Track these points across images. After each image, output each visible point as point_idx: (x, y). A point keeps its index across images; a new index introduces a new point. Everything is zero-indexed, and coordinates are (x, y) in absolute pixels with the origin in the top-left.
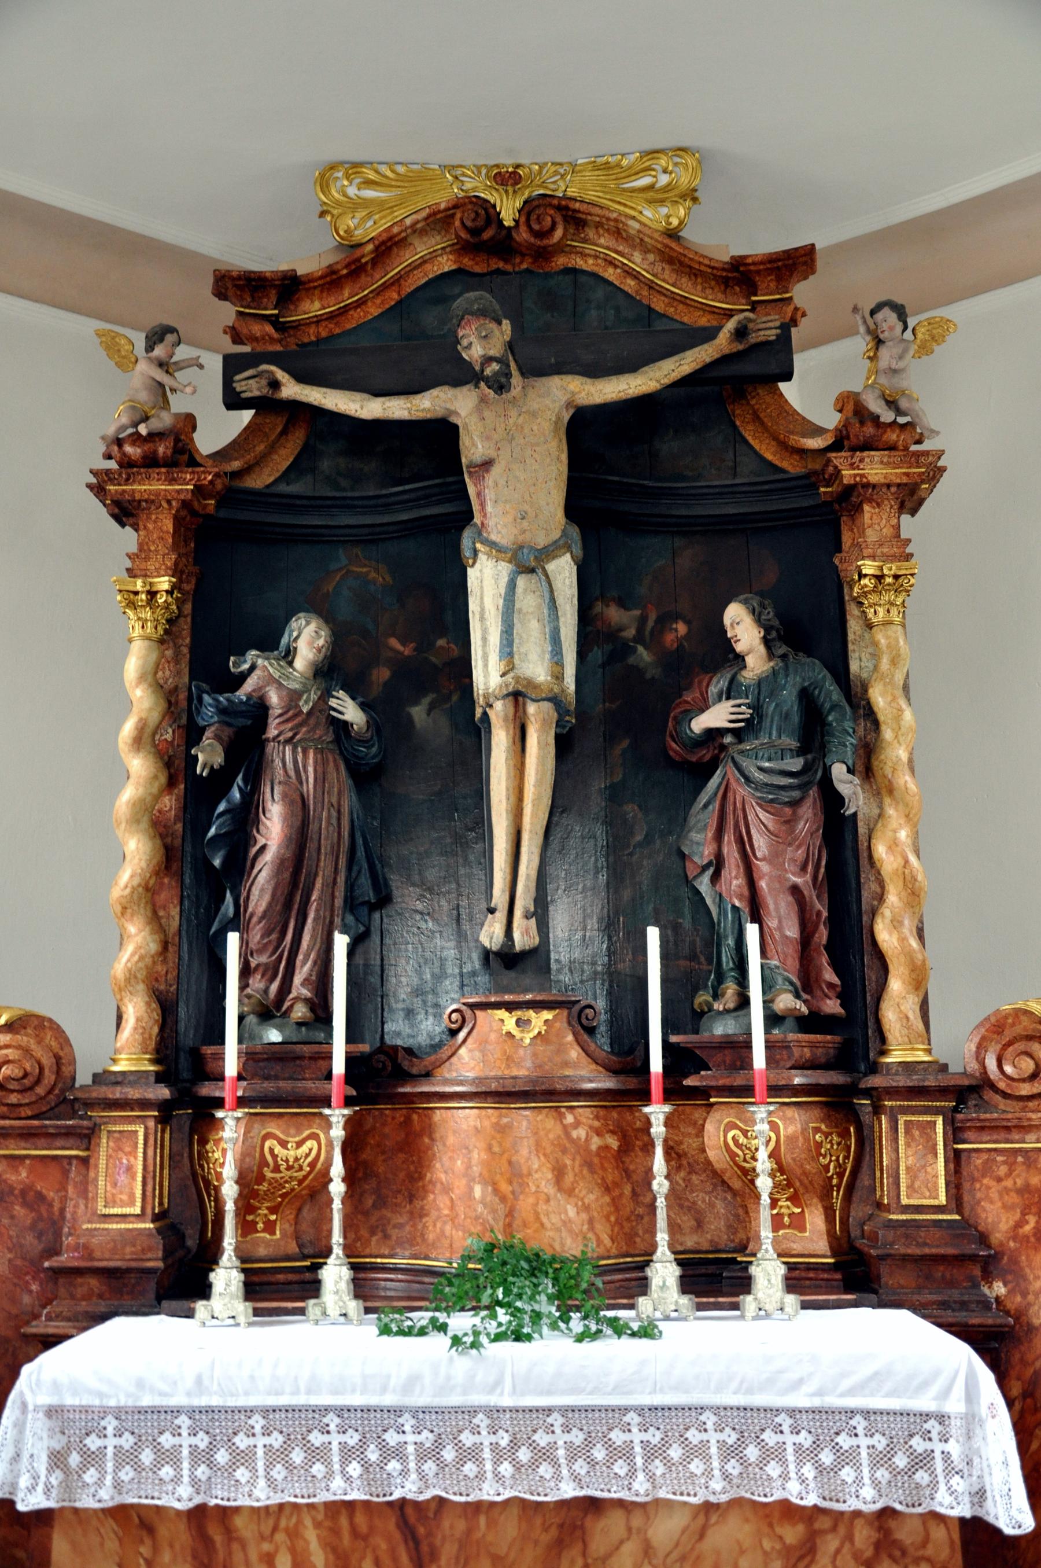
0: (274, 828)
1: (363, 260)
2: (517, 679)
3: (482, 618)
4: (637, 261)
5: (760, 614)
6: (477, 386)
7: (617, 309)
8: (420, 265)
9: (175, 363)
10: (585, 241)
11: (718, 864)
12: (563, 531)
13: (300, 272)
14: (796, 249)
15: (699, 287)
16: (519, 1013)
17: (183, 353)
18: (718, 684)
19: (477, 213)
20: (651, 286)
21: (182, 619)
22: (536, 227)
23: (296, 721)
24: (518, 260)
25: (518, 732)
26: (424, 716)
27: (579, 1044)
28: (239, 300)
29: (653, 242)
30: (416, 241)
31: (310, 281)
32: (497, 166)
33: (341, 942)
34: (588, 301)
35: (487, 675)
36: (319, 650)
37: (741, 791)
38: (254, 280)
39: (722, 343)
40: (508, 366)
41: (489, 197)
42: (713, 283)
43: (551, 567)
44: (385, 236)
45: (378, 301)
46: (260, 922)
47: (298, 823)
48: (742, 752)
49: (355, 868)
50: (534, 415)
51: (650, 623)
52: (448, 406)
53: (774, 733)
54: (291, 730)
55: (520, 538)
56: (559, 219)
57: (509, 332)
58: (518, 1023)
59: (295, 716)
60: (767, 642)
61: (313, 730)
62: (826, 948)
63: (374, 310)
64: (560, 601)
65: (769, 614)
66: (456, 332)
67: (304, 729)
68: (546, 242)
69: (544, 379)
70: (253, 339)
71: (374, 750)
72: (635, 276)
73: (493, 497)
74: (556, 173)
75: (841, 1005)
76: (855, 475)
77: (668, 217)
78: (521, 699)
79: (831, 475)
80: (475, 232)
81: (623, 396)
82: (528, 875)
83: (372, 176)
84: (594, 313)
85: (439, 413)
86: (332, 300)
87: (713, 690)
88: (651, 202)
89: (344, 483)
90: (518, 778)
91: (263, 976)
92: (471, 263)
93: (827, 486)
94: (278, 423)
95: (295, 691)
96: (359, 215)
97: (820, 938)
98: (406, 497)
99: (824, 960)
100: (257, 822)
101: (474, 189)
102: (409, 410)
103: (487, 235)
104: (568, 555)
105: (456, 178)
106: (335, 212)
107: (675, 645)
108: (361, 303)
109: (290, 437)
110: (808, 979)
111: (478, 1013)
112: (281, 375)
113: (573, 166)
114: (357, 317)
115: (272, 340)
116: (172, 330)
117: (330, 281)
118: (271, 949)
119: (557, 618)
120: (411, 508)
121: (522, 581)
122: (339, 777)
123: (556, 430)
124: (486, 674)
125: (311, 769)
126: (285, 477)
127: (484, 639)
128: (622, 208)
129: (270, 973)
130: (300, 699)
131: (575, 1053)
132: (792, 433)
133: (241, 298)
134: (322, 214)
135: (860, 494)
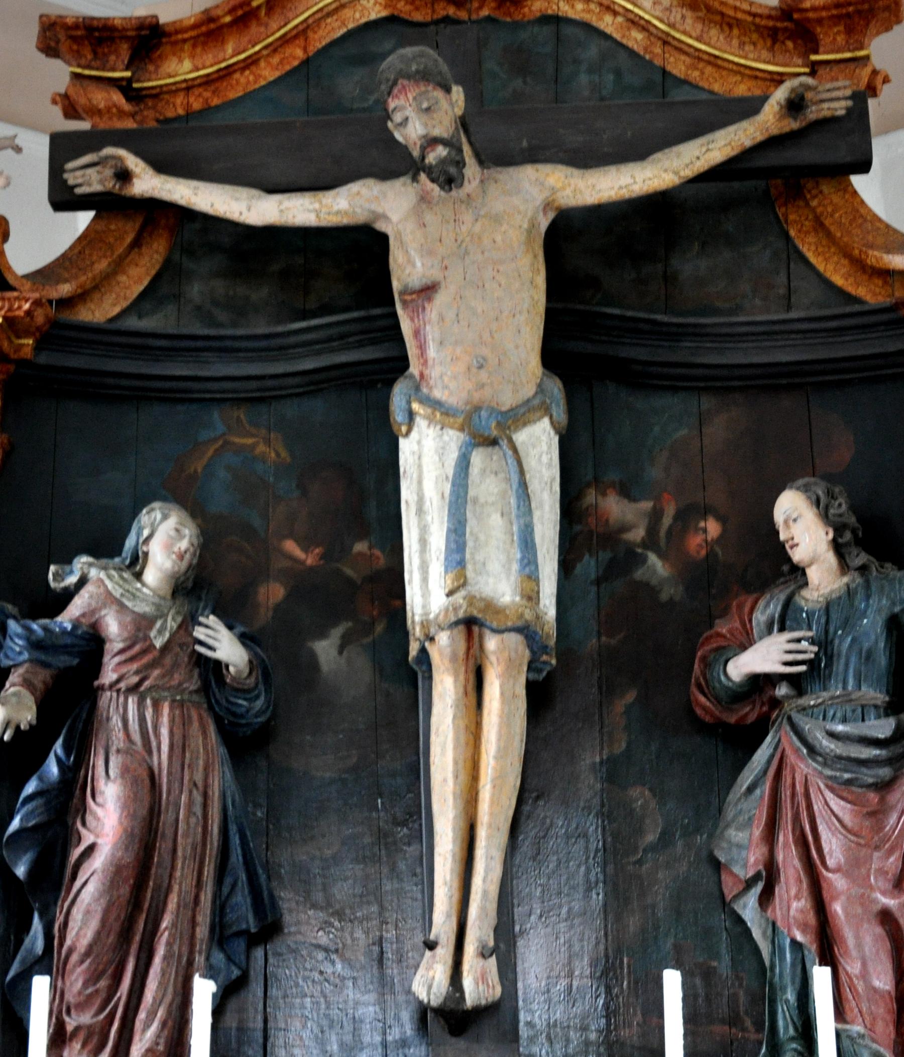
0: (107, 819)
2: (471, 600)
6: (415, 179)
7: (618, 73)
11: (768, 879)
15: (735, 42)
18: (767, 609)
20: (666, 41)
26: (334, 652)
28: (76, 57)
31: (177, 32)
33: (204, 991)
34: (576, 62)
35: (427, 594)
36: (181, 557)
37: (803, 768)
38: (97, 29)
39: (768, 120)
40: (460, 151)
42: (755, 36)
43: (521, 437)
45: (275, 60)
46: (82, 962)
47: (143, 812)
48: (803, 710)
49: (228, 881)
50: (497, 219)
51: (667, 521)
54: (137, 672)
55: (477, 396)
59: (144, 652)
60: (838, 547)
61: (169, 673)
63: (268, 73)
64: (534, 486)
65: (840, 506)
66: (385, 102)
67: (156, 673)
69: (511, 170)
70: (93, 112)
73: (437, 335)
78: (476, 629)
81: (626, 194)
85: (360, 217)
86: (209, 58)
87: (760, 617)
89: (222, 316)
90: (471, 746)
91: (84, 1046)
94: (129, 230)
100: (83, 809)
104: (546, 422)
107: (703, 553)
108: (251, 63)
109: (144, 249)
112: (133, 162)
114: (244, 83)
115: (122, 114)
118: (98, 1002)
119: (530, 511)
120: (319, 353)
121: (478, 458)
122: (207, 742)
123: (529, 241)
124: (426, 592)
125: (165, 732)
126: (136, 306)
127: (423, 542)
129: (95, 1040)
132: (871, 247)
133: (78, 54)
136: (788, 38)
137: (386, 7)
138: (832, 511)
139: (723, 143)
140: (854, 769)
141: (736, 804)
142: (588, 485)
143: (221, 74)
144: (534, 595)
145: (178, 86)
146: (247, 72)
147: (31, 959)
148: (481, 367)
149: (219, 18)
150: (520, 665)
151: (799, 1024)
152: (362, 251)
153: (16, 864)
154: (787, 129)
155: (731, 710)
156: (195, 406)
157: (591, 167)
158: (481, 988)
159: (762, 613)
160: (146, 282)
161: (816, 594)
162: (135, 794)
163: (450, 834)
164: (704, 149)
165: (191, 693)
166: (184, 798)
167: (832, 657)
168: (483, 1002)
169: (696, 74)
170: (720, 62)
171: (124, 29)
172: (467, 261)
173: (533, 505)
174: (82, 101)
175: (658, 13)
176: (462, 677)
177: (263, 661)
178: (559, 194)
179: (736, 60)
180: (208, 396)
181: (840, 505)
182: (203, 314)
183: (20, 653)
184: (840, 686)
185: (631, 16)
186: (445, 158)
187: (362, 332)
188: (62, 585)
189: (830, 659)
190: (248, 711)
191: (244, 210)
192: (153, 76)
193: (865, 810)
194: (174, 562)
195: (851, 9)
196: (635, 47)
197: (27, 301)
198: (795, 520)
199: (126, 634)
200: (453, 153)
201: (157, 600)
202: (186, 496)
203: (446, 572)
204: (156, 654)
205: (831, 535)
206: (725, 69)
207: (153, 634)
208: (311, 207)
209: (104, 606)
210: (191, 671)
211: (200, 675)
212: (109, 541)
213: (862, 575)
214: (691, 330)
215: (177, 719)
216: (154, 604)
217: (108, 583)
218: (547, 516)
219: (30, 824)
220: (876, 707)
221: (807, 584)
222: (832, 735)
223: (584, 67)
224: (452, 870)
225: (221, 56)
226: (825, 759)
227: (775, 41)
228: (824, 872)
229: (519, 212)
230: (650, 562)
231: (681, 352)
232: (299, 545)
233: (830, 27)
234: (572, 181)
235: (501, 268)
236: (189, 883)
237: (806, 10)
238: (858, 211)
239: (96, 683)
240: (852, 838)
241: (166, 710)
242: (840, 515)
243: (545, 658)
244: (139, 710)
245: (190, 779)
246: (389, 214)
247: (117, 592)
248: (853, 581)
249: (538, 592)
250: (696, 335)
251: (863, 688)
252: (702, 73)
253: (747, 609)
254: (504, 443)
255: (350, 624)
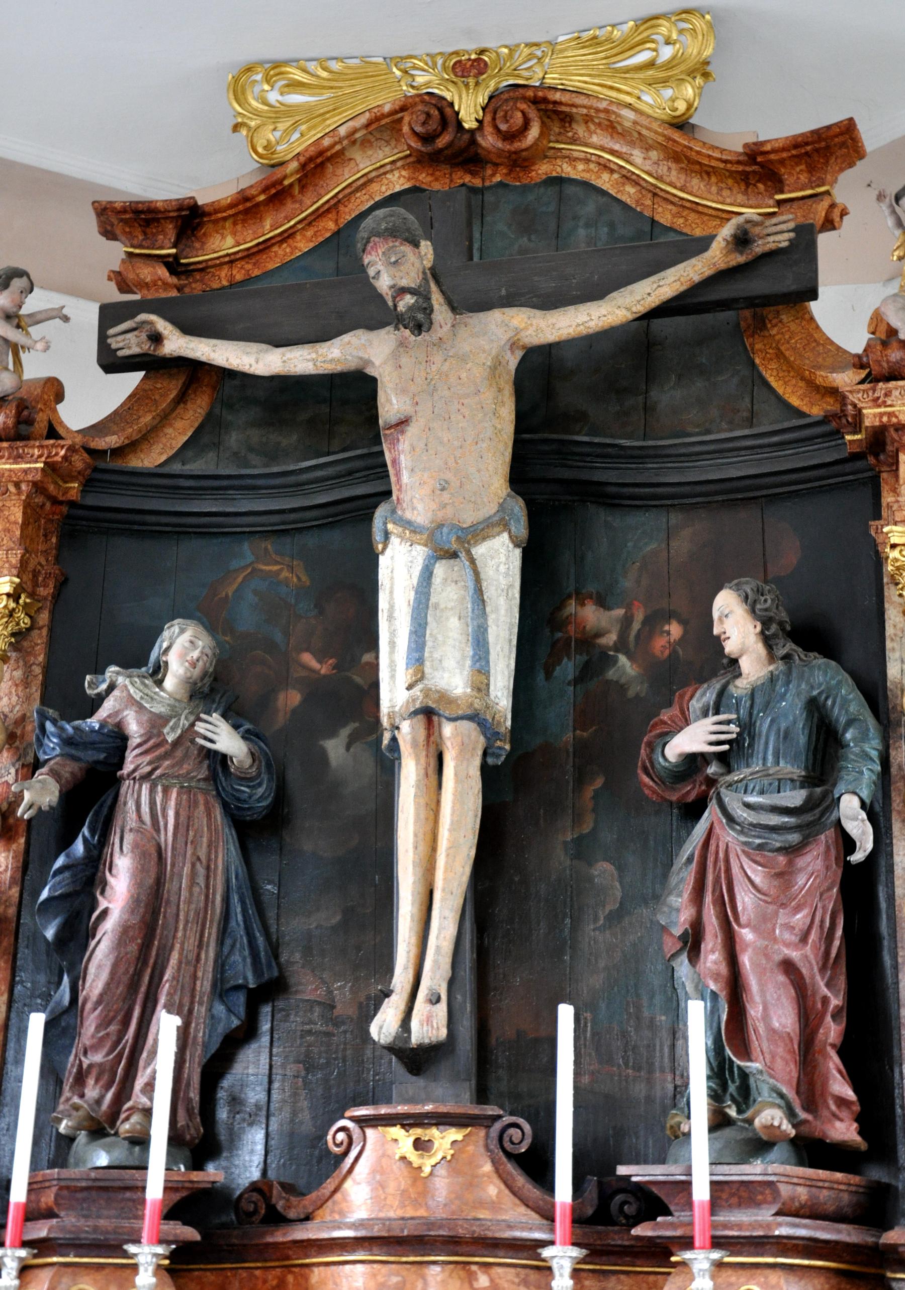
1: (286, 182)
2: (427, 692)
3: (391, 618)
4: (640, 162)
5: (755, 602)
7: (612, 226)
8: (364, 185)
9: (30, 316)
10: (574, 141)
11: (692, 942)
12: (501, 505)
13: (200, 202)
14: (828, 128)
15: (714, 189)
16: (417, 1132)
17: (34, 303)
18: (706, 695)
19: (428, 115)
20: (655, 194)
21: (35, 632)
22: (503, 127)
23: (157, 753)
24: (489, 172)
25: (433, 762)
26: (342, 750)
27: (500, 1176)
29: (652, 135)
30: (356, 154)
31: (216, 211)
32: (456, 53)
34: (576, 218)
35: (394, 693)
36: (194, 665)
37: (728, 837)
38: (142, 212)
39: (716, 256)
40: (428, 299)
41: (448, 96)
42: (730, 182)
43: (480, 551)
44: (312, 151)
45: (309, 233)
46: (95, 1009)
47: (150, 881)
48: (729, 785)
49: (228, 942)
50: (463, 359)
51: (636, 626)
52: (361, 354)
53: (770, 758)
54: (149, 764)
55: (440, 514)
56: (533, 114)
57: (430, 256)
58: (419, 1145)
59: (157, 746)
60: (767, 640)
61: (180, 764)
62: (843, 1051)
63: (303, 245)
64: (491, 592)
65: (767, 602)
66: (361, 259)
67: (167, 763)
68: (517, 145)
70: (143, 285)
71: (260, 791)
72: (635, 181)
73: (409, 464)
74: (531, 56)
75: (860, 1133)
76: (881, 415)
77: (673, 100)
78: (435, 718)
79: (854, 416)
80: (427, 139)
81: (583, 331)
82: (438, 948)
83: (299, 76)
84: (582, 232)
85: (351, 364)
86: (249, 233)
87: (696, 705)
88: (651, 83)
89: (254, 459)
91: (97, 1081)
92: (429, 179)
93: (855, 433)
94: (172, 388)
95: (159, 716)
96: (281, 127)
97: (827, 1034)
98: (320, 473)
99: (833, 1063)
101: (428, 84)
102: (314, 361)
103: (442, 141)
104: (505, 535)
105: (405, 72)
106: (253, 124)
107: (667, 652)
108: (287, 236)
109: (189, 405)
110: (813, 1095)
111: (370, 1132)
112: (162, 326)
113: (552, 44)
114: (282, 254)
116: (20, 273)
117: (245, 208)
118: (108, 1045)
119: (484, 614)
120: (332, 488)
121: (440, 570)
122: (212, 823)
125: (171, 814)
126: (180, 455)
128: (614, 94)
129: (106, 1077)
130: (165, 725)
131: (493, 1189)
132: (819, 368)
133: (130, 236)
134: (236, 128)
135: (893, 441)
136: (759, 181)
137: (409, 179)
138: (758, 606)
139: (673, 279)
140: (766, 835)
141: (678, 874)
142: (569, 597)
143: (261, 247)
144: (483, 687)
145: (222, 260)
146: (285, 245)
147: (59, 1010)
148: (443, 489)
149: (254, 197)
150: (474, 749)
151: (715, 1064)
152: (353, 393)
153: (45, 928)
154: (733, 263)
155: (674, 789)
156: (227, 540)
157: (556, 308)
158: (425, 1028)
159: (698, 701)
160: (190, 434)
161: (745, 682)
162: (143, 866)
163: (410, 898)
164: (655, 286)
165: (199, 780)
166: (186, 870)
167: (753, 739)
168: (427, 1041)
169: (681, 221)
170: (700, 209)
171: (166, 211)
172: (436, 398)
173: (488, 609)
174: (131, 276)
175: (647, 168)
176: (423, 760)
177: (266, 754)
178: (523, 334)
179: (714, 205)
180: (238, 530)
181: (766, 601)
182: (238, 458)
183: (54, 749)
184: (760, 762)
185: (625, 172)
186: (413, 305)
187: (367, 468)
188: (96, 691)
189: (752, 738)
190: (250, 797)
191: (253, 363)
192: (200, 252)
193: (773, 871)
194: (187, 669)
195: (809, 148)
196: (629, 201)
197: (62, 447)
198: (726, 616)
199: (142, 732)
200: (421, 300)
201: (172, 702)
202: (212, 619)
203: (407, 669)
204: (168, 747)
205: (759, 628)
206: (706, 214)
207: (165, 731)
208: (309, 357)
209: (126, 708)
210: (201, 762)
211: (209, 766)
212: (138, 655)
213: (786, 663)
214: (651, 452)
215: (184, 802)
216: (169, 705)
217: (130, 687)
218: (502, 619)
219: (57, 894)
220: (792, 780)
221: (740, 675)
222: (748, 806)
223: (581, 223)
224: (411, 929)
225: (260, 231)
226: (743, 827)
227: (748, 185)
228: (736, 927)
229: (484, 351)
230: (620, 664)
231: (650, 473)
232: (315, 656)
233: (792, 167)
234: (534, 322)
235: (465, 401)
236: (191, 943)
237: (767, 153)
238: (812, 336)
239: (119, 773)
240: (763, 897)
241: (174, 795)
242: (766, 610)
243: (499, 743)
244: (150, 795)
245: (194, 854)
246: (373, 359)
247: (138, 696)
248: (777, 669)
249: (488, 685)
250: (656, 456)
251: (782, 763)
252: (687, 220)
253: (687, 698)
254: (463, 555)
255: (357, 725)
